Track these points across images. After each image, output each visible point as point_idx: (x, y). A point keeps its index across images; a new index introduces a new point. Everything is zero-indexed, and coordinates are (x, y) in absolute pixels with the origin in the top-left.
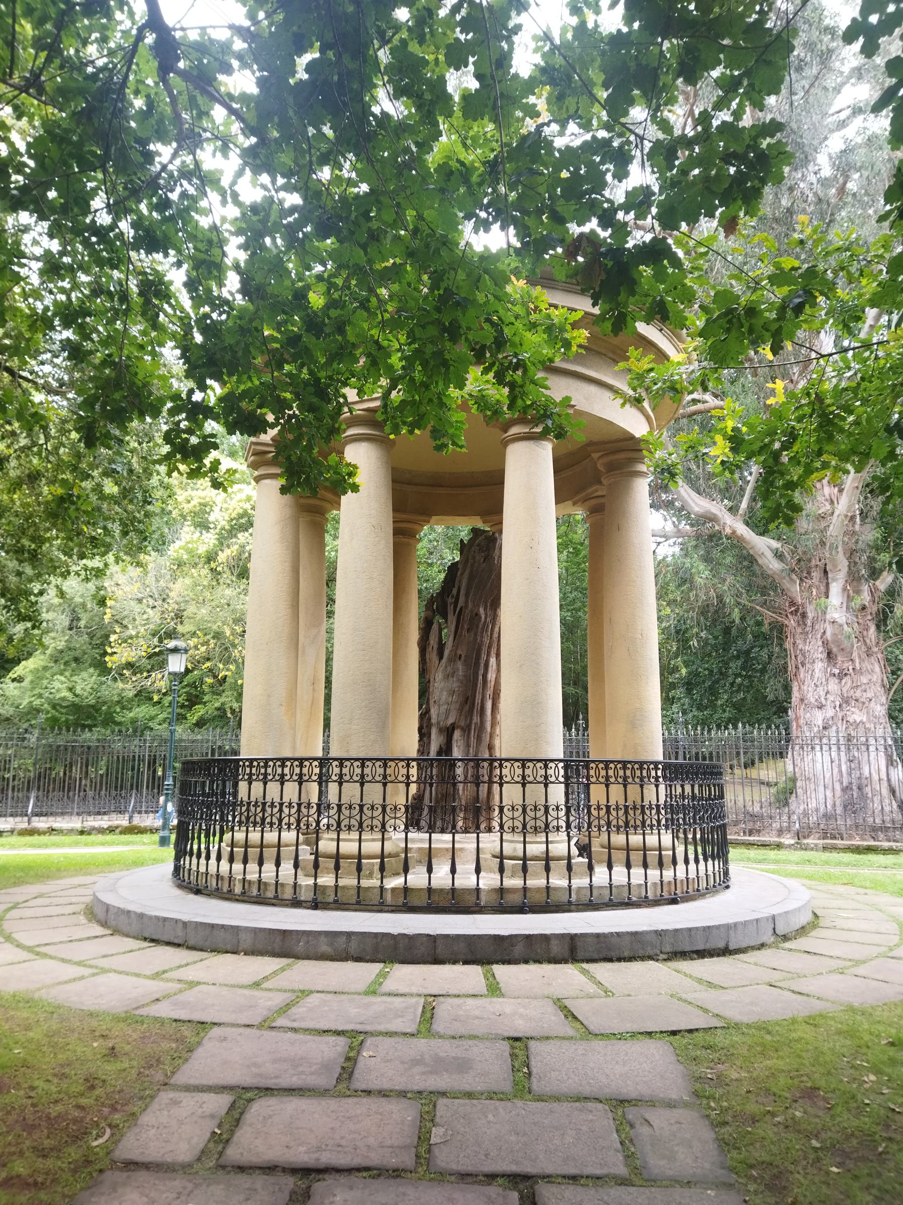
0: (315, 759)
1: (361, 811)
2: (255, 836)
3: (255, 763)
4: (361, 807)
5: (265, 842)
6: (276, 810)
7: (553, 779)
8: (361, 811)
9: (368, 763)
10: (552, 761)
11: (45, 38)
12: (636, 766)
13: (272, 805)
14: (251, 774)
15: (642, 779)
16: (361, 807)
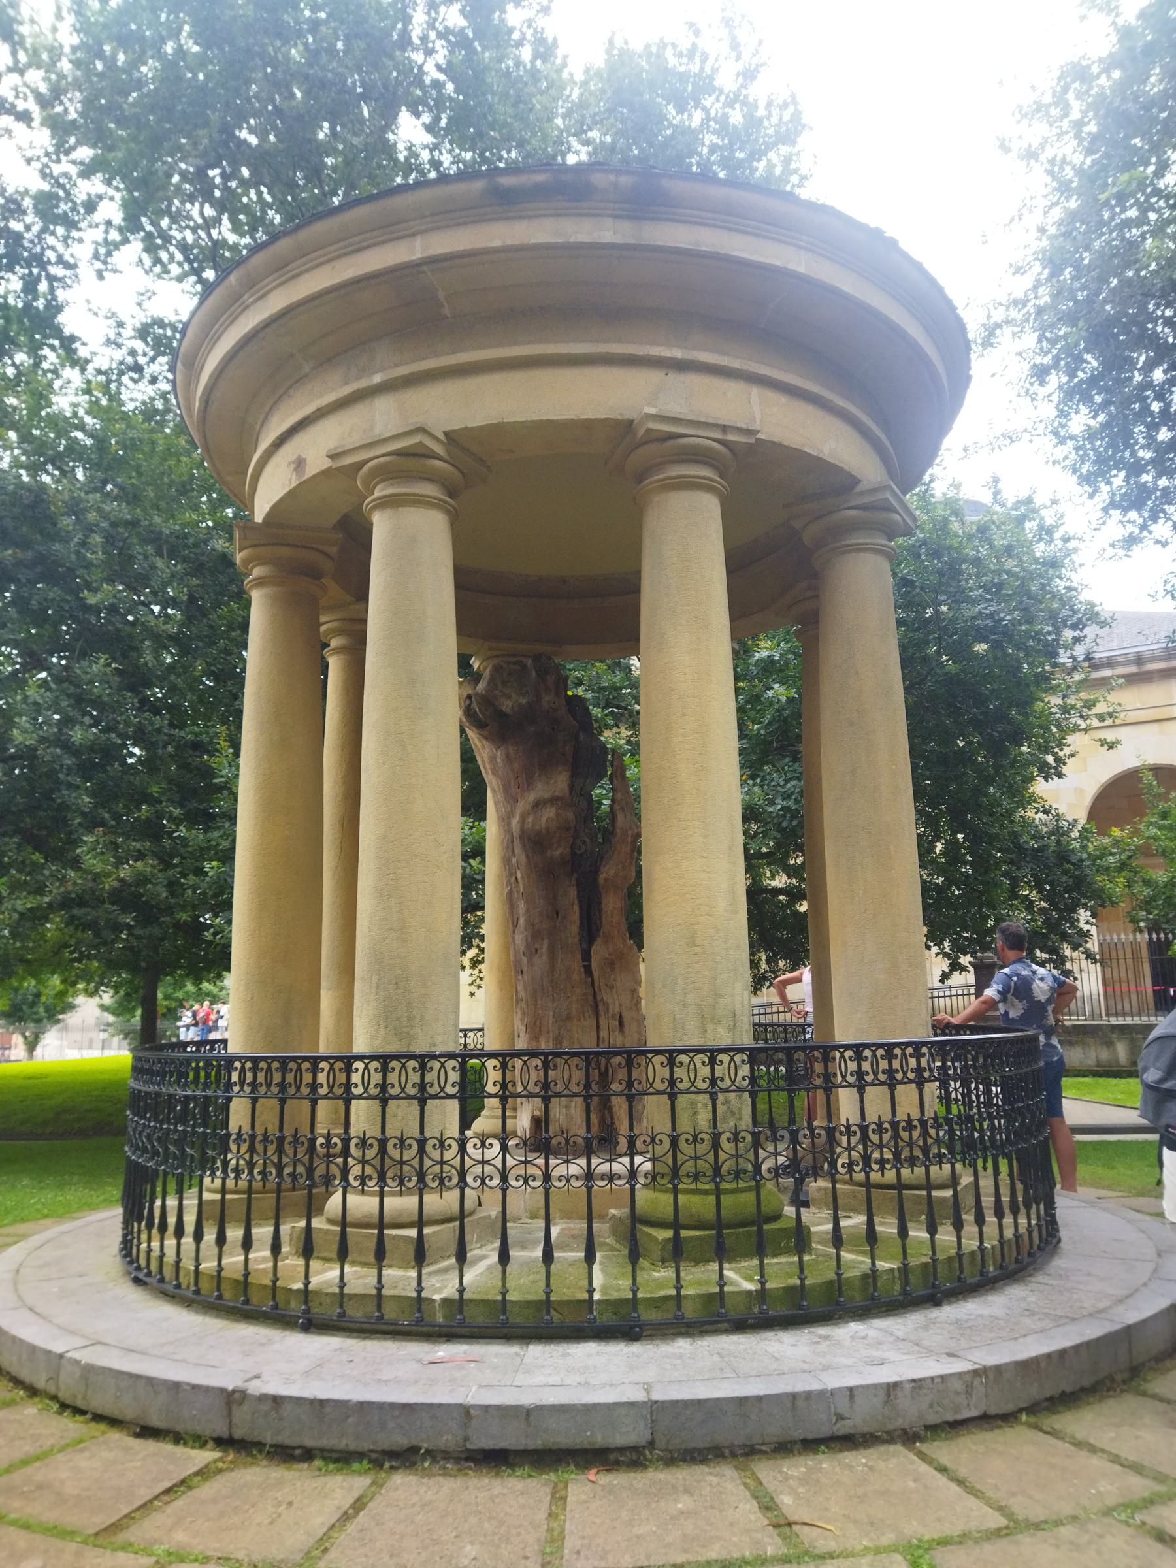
0: (740, 1050)
1: (422, 1151)
2: (400, 1204)
3: (263, 1065)
4: (422, 1143)
5: (349, 1219)
6: (916, 1134)
7: (869, 1078)
8: (422, 1151)
9: (394, 1064)
10: (435, 1057)
11: (97, 98)
12: (880, 1052)
13: (909, 1126)
14: (919, 1070)
15: (283, 1087)
16: (422, 1143)
